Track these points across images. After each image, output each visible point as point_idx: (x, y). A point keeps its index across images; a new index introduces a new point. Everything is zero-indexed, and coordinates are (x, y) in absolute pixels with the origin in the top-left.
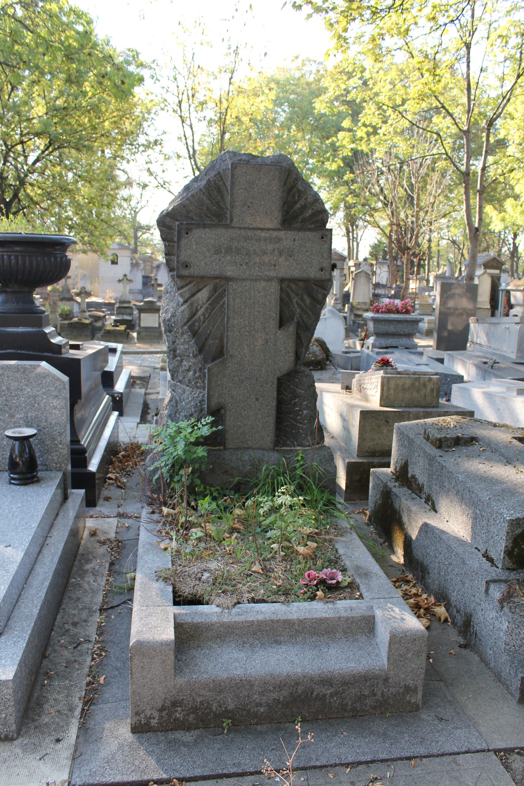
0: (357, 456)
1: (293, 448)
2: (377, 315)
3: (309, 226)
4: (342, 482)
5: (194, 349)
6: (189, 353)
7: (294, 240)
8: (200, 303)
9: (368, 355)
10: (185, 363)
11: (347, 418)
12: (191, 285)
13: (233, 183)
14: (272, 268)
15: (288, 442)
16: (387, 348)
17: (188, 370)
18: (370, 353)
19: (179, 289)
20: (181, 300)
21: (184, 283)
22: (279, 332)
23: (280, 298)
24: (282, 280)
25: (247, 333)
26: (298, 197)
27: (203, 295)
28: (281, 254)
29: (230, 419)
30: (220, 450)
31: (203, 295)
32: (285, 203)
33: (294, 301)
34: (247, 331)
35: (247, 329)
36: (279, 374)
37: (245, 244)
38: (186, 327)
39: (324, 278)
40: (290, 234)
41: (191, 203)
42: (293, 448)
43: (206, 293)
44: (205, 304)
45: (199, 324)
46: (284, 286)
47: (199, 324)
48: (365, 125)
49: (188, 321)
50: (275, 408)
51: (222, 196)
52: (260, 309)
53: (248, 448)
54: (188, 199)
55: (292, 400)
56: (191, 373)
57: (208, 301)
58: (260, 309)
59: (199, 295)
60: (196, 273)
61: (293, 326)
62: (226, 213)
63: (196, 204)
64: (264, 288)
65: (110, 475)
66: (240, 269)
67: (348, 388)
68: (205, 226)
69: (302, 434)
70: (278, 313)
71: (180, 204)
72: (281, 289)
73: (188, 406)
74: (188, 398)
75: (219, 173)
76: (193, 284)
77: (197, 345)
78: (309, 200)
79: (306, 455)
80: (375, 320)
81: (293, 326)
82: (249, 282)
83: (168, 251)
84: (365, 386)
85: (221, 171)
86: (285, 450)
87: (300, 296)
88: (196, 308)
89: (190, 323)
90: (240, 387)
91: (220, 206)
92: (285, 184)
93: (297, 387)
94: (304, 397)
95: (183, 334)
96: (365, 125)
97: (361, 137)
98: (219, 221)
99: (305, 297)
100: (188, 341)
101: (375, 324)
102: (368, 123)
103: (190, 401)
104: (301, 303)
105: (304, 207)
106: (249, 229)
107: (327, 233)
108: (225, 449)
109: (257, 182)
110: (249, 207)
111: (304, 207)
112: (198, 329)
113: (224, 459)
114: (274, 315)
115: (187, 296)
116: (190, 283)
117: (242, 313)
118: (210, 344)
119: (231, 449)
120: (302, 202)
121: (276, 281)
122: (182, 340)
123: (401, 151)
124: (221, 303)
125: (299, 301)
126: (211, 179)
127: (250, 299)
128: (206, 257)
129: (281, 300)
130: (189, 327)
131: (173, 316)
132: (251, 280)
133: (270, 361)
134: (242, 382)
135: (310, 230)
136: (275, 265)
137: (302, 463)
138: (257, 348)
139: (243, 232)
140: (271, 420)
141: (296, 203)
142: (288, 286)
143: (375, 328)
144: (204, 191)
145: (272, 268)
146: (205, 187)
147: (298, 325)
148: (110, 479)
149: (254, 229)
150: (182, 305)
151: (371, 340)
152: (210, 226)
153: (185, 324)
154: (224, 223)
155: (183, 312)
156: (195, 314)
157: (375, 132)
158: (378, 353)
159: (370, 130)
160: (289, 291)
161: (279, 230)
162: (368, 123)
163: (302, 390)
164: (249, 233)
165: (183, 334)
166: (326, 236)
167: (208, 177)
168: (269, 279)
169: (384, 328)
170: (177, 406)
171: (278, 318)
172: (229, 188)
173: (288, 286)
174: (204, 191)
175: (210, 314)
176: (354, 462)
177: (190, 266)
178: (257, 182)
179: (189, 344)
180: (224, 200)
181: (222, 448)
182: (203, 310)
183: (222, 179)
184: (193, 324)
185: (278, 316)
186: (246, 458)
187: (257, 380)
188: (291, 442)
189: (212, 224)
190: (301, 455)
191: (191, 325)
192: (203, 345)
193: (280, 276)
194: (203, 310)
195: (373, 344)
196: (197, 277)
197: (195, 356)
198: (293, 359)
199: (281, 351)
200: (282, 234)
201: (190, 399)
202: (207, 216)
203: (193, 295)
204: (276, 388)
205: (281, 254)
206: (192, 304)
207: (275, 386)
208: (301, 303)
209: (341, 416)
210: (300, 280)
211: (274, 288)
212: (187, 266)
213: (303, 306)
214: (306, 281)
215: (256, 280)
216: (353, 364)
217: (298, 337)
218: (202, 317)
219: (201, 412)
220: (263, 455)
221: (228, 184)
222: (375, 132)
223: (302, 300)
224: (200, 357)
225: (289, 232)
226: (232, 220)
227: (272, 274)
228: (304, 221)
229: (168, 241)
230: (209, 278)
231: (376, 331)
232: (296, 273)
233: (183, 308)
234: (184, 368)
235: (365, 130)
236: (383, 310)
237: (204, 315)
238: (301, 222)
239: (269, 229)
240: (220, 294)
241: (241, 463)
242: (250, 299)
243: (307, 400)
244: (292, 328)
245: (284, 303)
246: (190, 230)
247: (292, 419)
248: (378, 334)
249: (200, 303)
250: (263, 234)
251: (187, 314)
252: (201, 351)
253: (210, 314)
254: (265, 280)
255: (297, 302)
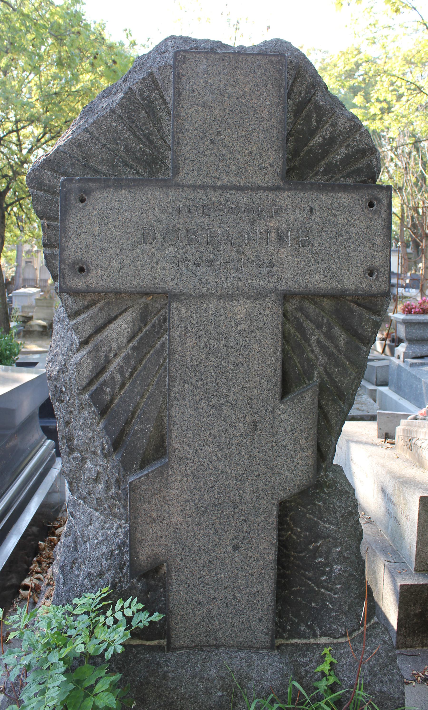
0: (416, 570)
1: (312, 641)
2: (409, 317)
3: (342, 181)
4: (391, 612)
5: (103, 441)
6: (96, 447)
7: (311, 210)
8: (114, 345)
9: (399, 366)
10: (89, 465)
11: (395, 499)
12: (94, 310)
13: (178, 93)
14: (264, 270)
15: (303, 628)
16: (422, 357)
17: (96, 480)
18: (402, 364)
19: (71, 316)
20: (76, 340)
21: (80, 304)
22: (282, 407)
23: (283, 333)
24: (286, 297)
25: (212, 411)
26: (318, 122)
27: (119, 330)
28: (282, 239)
29: (179, 592)
30: (160, 648)
31: (119, 330)
32: (289, 135)
33: (313, 339)
34: (213, 406)
35: (213, 401)
36: (281, 495)
37: (206, 220)
38: (86, 396)
39: (375, 289)
40: (305, 198)
41: (93, 137)
42: (312, 641)
43: (125, 326)
44: (124, 347)
45: (113, 389)
46: (290, 307)
47: (113, 389)
48: (378, 100)
49: (90, 383)
50: (273, 565)
51: (157, 123)
52: (240, 359)
53: (217, 646)
54: (86, 130)
55: (311, 542)
56: (101, 486)
57: (129, 341)
58: (240, 359)
59: (111, 329)
60: (101, 285)
61: (310, 392)
62: (165, 157)
63: (104, 141)
64: (249, 314)
65: (27, 581)
66: (195, 274)
67: (388, 436)
68: (119, 184)
69: (332, 610)
70: (279, 366)
71: (70, 141)
72: (284, 315)
73: (96, 554)
74: (96, 537)
75: (151, 75)
76: (98, 306)
77: (108, 433)
78: (340, 127)
79: (339, 660)
80: (407, 323)
81: (310, 392)
82: (215, 302)
83: (49, 239)
84: (419, 443)
85: (155, 70)
86: (297, 645)
87: (324, 329)
88: (106, 356)
89: (93, 388)
90: (199, 524)
91: (152, 142)
92: (289, 97)
93: (320, 518)
94: (336, 539)
95: (81, 408)
96: (378, 100)
97: (375, 115)
98: (151, 174)
99: (337, 330)
100: (92, 424)
101: (406, 327)
102: (382, 99)
103: (101, 543)
104: (327, 343)
105: (330, 143)
106: (214, 188)
107: (382, 195)
108: (170, 647)
109: (229, 89)
110: (212, 142)
111: (330, 143)
112: (112, 401)
113: (165, 676)
114: (270, 372)
115: (87, 330)
116: (93, 303)
117: (202, 368)
118: (137, 431)
119: (181, 648)
120: (326, 131)
121: (274, 298)
122: (81, 421)
123: (418, 130)
124: (157, 346)
125: (322, 338)
126: (134, 89)
127: (217, 339)
128: (121, 249)
129: (286, 337)
130: (92, 396)
131: (62, 371)
132: (219, 297)
133: (262, 469)
134: (204, 512)
135: (345, 188)
136: (271, 265)
137: (332, 680)
138: (234, 441)
139: (200, 194)
140: (267, 588)
141: (312, 133)
142: (301, 309)
143: (407, 333)
144: (121, 113)
145: (264, 270)
146: (121, 104)
147: (322, 387)
148: (26, 588)
149: (223, 188)
150: (78, 350)
151: (401, 349)
152: (130, 184)
153: (85, 389)
154: (161, 176)
155: (79, 364)
156: (103, 370)
157: (389, 110)
158: (412, 365)
159: (385, 105)
160: (302, 319)
161: (278, 188)
162: (382, 99)
163: (331, 523)
164: (215, 197)
165: (81, 408)
166: (379, 201)
167: (128, 84)
168: (259, 296)
169: (418, 333)
170: (76, 549)
171: (279, 377)
172: (170, 105)
173: (301, 309)
174: (121, 113)
175: (135, 369)
176: (411, 585)
177: (89, 270)
178: (229, 89)
179: (94, 431)
180: (160, 130)
181: (163, 642)
182: (119, 360)
183: (157, 87)
184: (100, 390)
185: (279, 372)
186: (213, 672)
187: (235, 507)
188: (309, 627)
189: (135, 180)
190: (329, 659)
191: (95, 392)
192: (122, 433)
193: (282, 287)
194: (119, 360)
195: (404, 353)
196: (106, 293)
197: (106, 456)
198: (311, 462)
199: (285, 446)
200: (284, 198)
201: (100, 539)
202: (125, 164)
203: (98, 330)
204: (275, 525)
205: (282, 239)
206: (97, 348)
207: (274, 519)
208: (327, 343)
209: (383, 491)
210: (324, 296)
211: (270, 313)
212: (81, 270)
213: (332, 348)
214: (338, 297)
215: (231, 297)
216: (379, 376)
217: (322, 414)
218: (119, 376)
219: (121, 568)
220: (250, 665)
221: (169, 95)
222: (389, 110)
223: (330, 337)
224: (116, 458)
225: (301, 194)
226: (176, 170)
227: (267, 284)
228: (330, 170)
229: (48, 219)
230: (130, 294)
231: (409, 337)
232: (317, 281)
233: (79, 355)
234: (87, 474)
235: (379, 106)
236: (417, 310)
237: (121, 371)
238: (326, 172)
239: (258, 189)
240: (153, 326)
241: (201, 686)
242: (217, 339)
243: (341, 545)
244: (308, 397)
245: (291, 344)
246: (88, 192)
247: (309, 579)
248: (411, 341)
249: (114, 345)
250: (245, 199)
251: (87, 371)
252: (116, 445)
253: (135, 369)
254: (249, 297)
255: (318, 342)
